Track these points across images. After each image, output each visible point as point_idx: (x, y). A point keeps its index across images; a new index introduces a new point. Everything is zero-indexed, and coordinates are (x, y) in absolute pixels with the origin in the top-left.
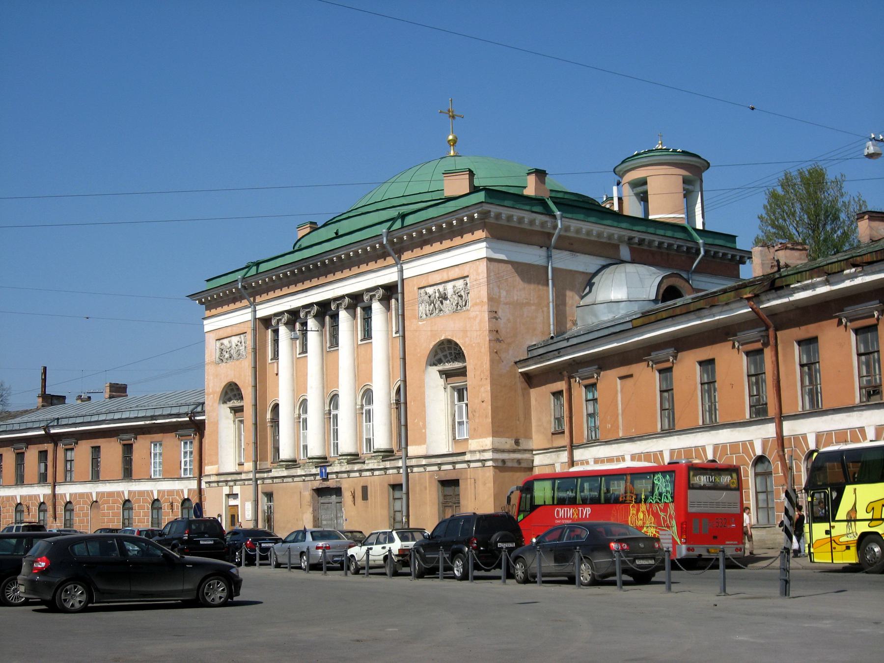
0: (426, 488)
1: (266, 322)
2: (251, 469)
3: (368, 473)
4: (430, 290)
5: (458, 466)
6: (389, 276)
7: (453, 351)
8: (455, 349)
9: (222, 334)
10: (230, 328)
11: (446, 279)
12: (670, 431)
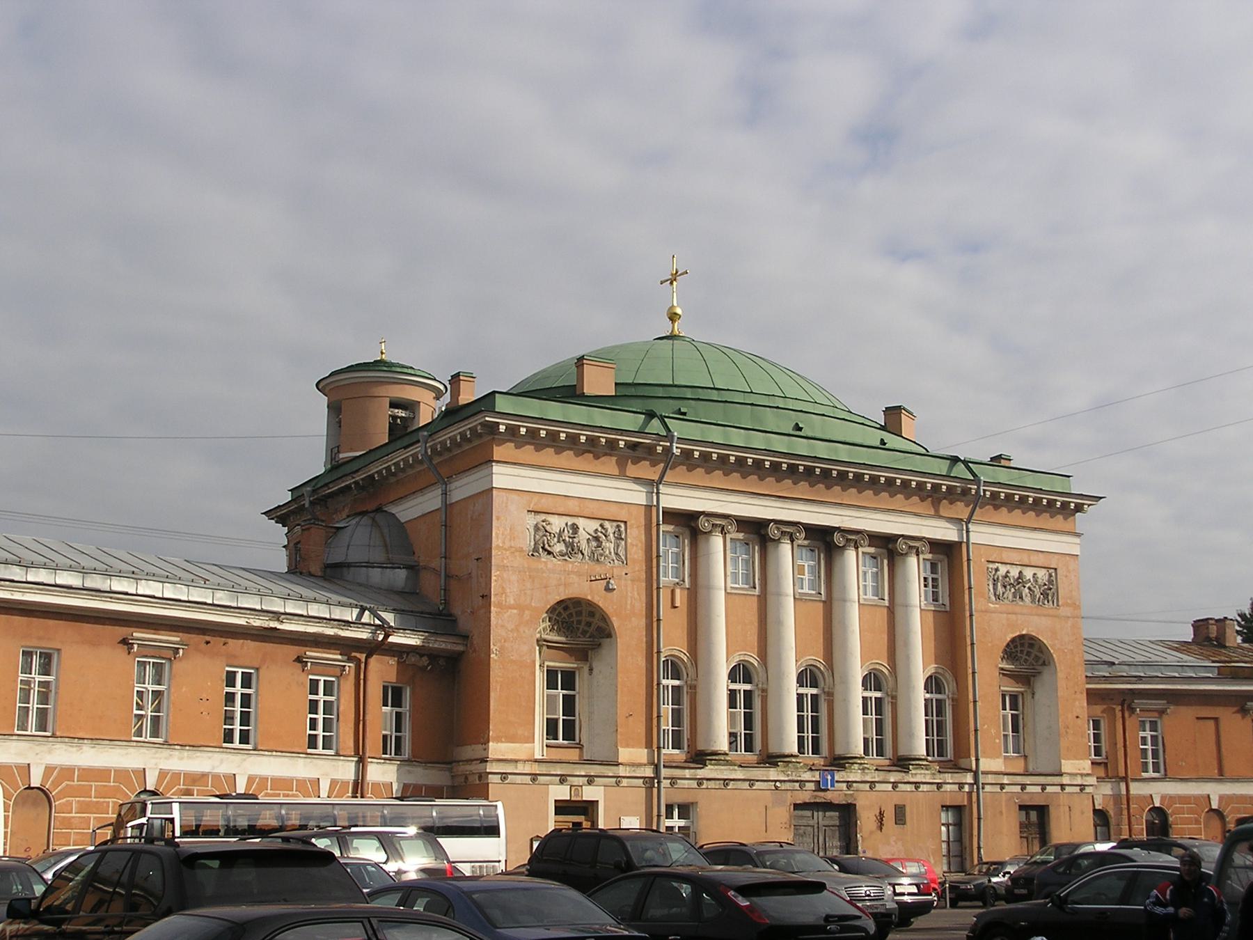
0: (1001, 813)
1: (689, 525)
2: (645, 760)
3: (909, 788)
4: (1003, 570)
5: (1049, 789)
6: (945, 532)
7: (564, 615)
8: (566, 608)
9: (545, 504)
10: (550, 499)
11: (1026, 562)
12: (1221, 776)
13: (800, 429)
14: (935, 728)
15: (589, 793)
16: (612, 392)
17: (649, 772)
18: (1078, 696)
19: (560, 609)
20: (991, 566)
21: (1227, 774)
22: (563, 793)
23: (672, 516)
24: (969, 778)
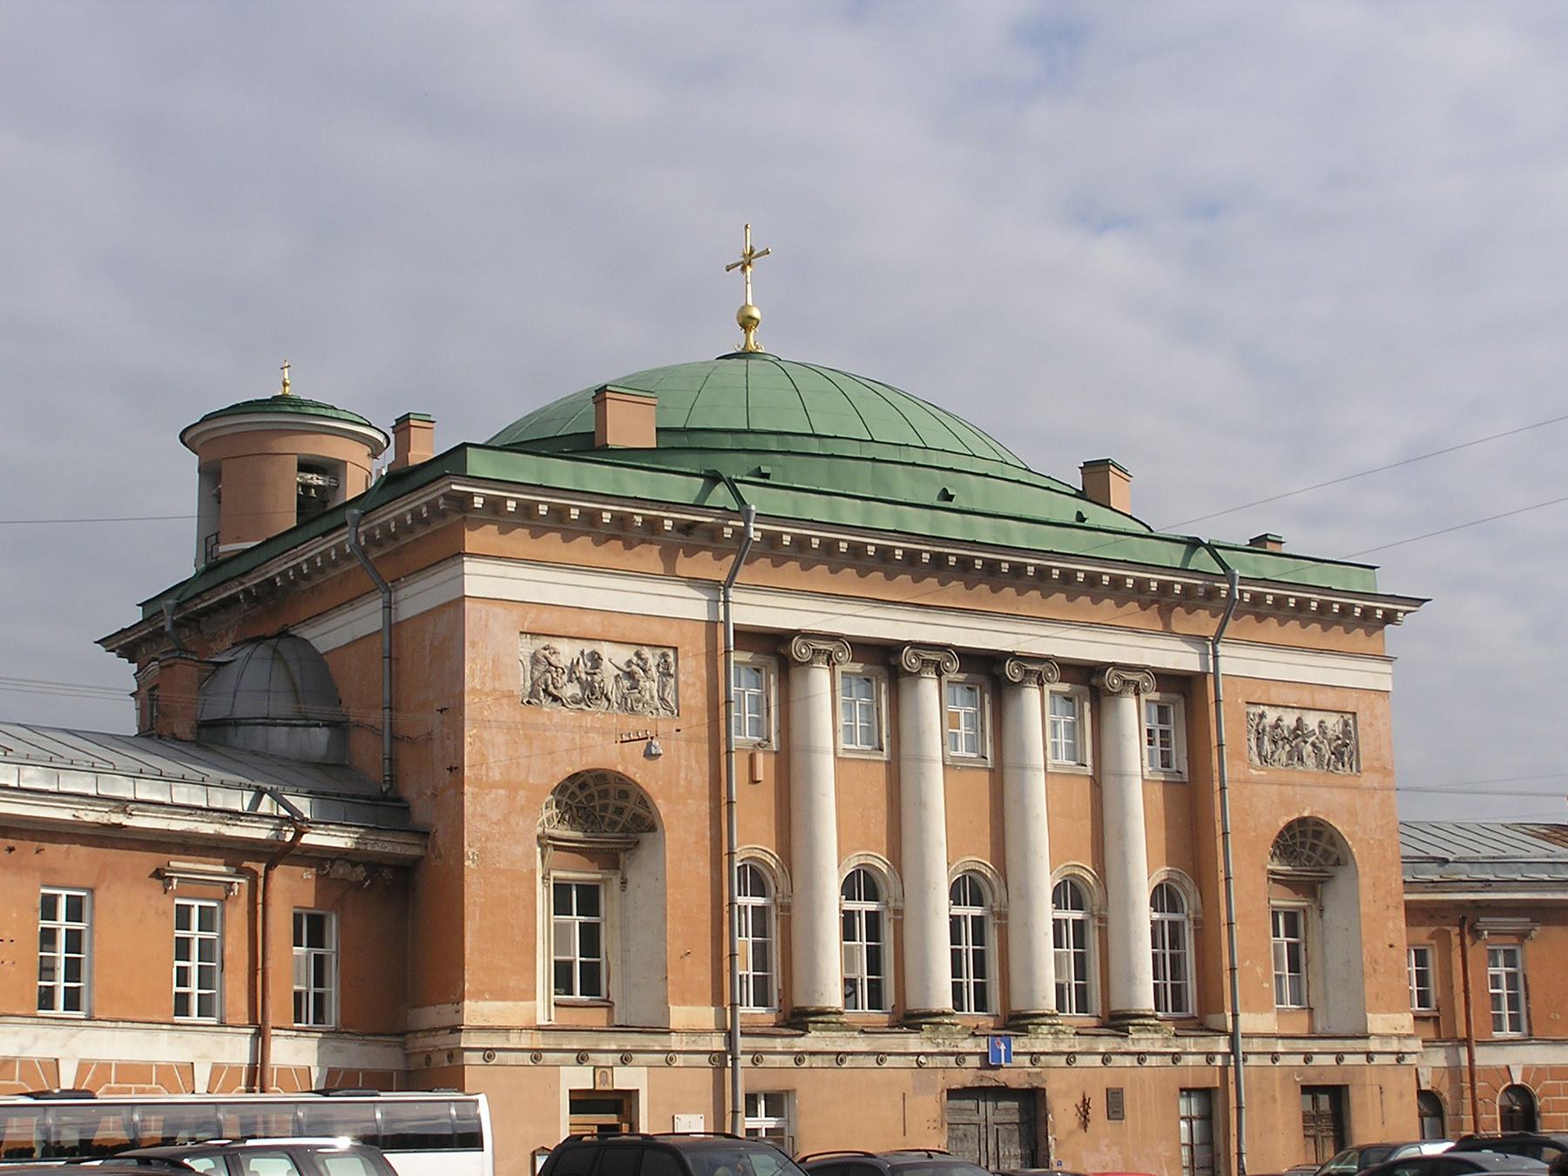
13: (950, 498)
14: (1168, 966)
17: (718, 1043)
18: (1392, 912)
23: (750, 638)
24: (1222, 1045)
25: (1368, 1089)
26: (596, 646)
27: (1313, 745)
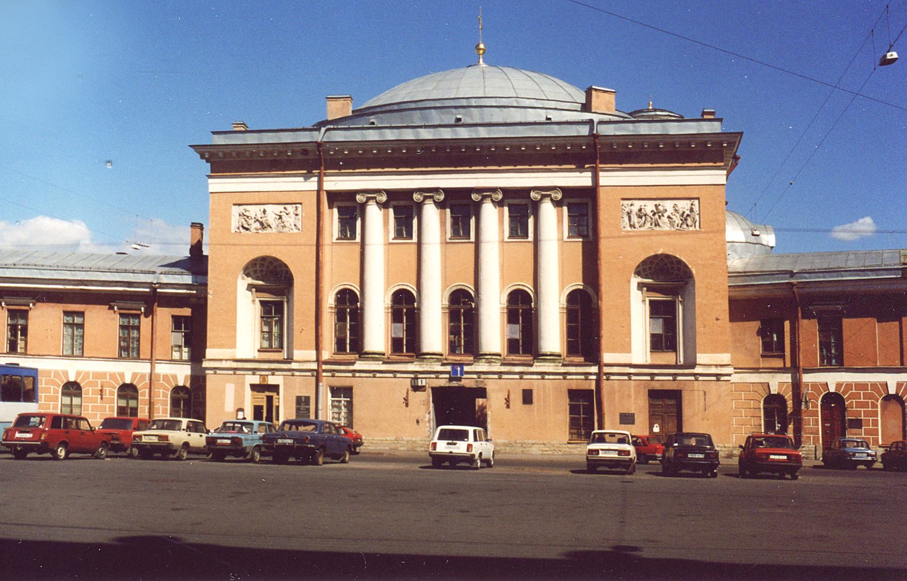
6: (583, 179)
13: (550, 119)
14: (571, 332)
15: (272, 380)
16: (351, 114)
17: (314, 366)
18: (719, 301)
19: (258, 263)
20: (626, 202)
21: (141, 357)
22: (256, 380)
23: (335, 197)
24: (594, 369)
25: (696, 393)
26: (266, 207)
27: (669, 217)
